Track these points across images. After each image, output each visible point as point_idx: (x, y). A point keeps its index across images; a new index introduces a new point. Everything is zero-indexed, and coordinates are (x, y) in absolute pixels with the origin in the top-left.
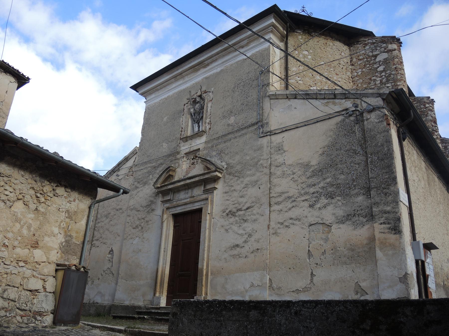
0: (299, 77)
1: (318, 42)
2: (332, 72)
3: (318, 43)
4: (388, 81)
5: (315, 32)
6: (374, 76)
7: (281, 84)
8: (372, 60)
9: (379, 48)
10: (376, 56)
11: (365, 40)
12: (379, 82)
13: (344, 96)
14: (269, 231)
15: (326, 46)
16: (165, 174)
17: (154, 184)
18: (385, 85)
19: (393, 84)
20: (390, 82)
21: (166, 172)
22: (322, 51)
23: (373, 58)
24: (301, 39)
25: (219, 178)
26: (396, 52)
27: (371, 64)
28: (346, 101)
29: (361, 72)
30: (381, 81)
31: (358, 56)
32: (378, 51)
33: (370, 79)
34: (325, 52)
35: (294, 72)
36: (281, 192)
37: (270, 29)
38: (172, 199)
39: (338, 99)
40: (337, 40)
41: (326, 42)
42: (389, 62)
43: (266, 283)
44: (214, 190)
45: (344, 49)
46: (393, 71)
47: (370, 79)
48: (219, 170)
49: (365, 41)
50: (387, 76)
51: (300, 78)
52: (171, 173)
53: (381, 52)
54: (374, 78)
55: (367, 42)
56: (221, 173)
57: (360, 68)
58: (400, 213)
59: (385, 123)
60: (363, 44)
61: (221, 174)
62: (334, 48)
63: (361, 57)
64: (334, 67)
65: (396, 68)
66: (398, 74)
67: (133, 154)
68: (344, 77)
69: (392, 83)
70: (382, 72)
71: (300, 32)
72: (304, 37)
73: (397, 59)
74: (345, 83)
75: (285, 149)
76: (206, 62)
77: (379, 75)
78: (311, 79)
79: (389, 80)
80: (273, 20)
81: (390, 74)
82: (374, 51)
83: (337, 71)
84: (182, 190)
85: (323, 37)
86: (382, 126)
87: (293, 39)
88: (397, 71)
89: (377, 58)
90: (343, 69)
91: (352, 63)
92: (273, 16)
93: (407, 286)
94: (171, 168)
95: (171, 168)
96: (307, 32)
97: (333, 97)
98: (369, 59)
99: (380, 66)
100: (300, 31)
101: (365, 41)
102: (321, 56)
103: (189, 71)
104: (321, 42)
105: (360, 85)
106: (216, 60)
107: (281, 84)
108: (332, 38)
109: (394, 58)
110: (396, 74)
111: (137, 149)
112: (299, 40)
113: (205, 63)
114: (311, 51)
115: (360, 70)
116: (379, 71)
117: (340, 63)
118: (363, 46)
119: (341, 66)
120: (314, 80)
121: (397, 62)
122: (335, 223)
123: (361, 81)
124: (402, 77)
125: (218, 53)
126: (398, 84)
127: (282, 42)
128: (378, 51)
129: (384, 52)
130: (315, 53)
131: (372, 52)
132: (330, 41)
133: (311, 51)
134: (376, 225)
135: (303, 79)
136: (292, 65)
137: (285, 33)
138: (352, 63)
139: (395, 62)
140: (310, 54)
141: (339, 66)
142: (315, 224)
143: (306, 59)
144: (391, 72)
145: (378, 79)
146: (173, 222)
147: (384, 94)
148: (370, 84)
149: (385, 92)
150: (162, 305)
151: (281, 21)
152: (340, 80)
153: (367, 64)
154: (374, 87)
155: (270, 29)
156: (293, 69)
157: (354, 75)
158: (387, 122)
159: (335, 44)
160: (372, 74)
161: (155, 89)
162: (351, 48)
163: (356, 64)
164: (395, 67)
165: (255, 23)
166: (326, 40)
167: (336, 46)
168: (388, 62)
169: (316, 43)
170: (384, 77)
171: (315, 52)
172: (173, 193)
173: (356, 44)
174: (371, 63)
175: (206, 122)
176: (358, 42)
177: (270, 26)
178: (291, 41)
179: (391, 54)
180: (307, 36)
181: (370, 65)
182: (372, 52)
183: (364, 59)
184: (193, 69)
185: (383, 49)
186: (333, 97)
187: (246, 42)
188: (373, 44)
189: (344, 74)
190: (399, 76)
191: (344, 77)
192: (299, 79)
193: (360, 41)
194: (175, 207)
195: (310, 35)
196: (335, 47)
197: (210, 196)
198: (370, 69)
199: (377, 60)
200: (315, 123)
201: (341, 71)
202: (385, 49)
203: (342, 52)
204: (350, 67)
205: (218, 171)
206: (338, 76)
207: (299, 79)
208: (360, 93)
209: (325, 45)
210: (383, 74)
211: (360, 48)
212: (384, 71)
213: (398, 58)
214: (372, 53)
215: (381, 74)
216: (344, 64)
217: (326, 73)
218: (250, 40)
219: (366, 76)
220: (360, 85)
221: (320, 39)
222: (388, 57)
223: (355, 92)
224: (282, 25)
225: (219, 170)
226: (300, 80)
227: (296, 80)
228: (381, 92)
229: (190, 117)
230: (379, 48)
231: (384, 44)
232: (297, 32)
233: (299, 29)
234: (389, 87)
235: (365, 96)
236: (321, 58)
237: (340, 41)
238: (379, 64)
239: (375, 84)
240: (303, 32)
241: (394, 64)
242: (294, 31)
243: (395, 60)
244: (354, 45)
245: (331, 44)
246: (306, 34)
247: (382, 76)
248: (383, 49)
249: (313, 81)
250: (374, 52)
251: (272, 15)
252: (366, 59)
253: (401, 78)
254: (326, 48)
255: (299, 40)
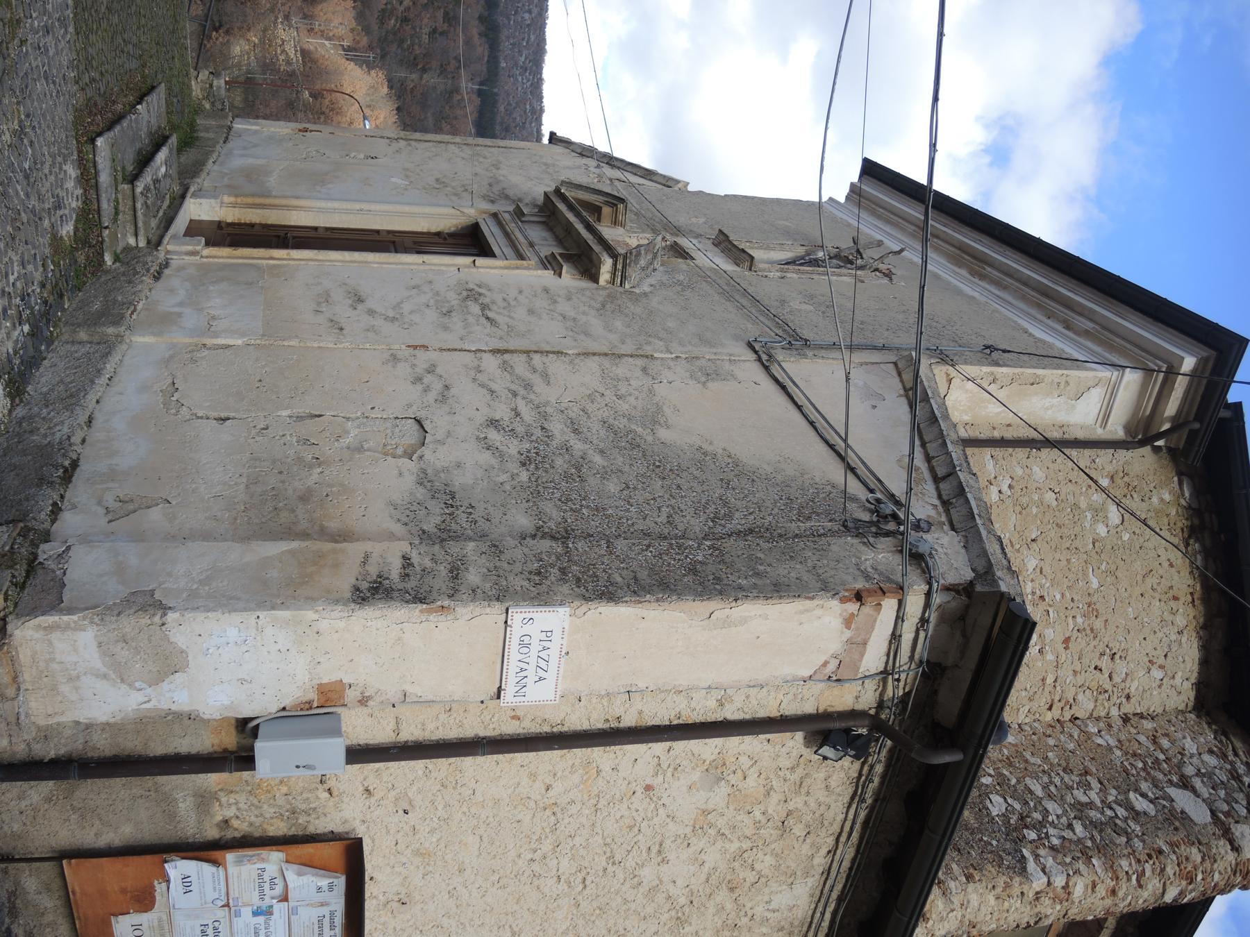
0: (1010, 487)
1: (1171, 565)
2: (1070, 620)
3: (1166, 564)
4: (1092, 825)
5: (1206, 552)
6: (1101, 783)
7: (967, 427)
8: (1165, 775)
9: (1222, 796)
10: (1185, 784)
11: (1241, 753)
12: (1084, 799)
13: (951, 496)
14: (403, 347)
15: (1164, 598)
16: (601, 198)
17: (567, 183)
18: (1075, 818)
19: (1089, 844)
20: (1095, 833)
21: (609, 200)
22: (1139, 578)
23: (1175, 779)
24: (1162, 500)
25: (594, 278)
26: (1226, 852)
27: (1148, 773)
28: (935, 506)
29: (1104, 743)
30: (1087, 804)
31: (1166, 735)
32: (1210, 794)
33: (1087, 772)
34: (1138, 591)
35: (1027, 471)
36: (550, 373)
37: (1157, 365)
38: (523, 219)
39: (937, 489)
40: (1205, 648)
41: (1182, 600)
42: (1176, 829)
43: (292, 553)
44: (553, 269)
45: (1178, 681)
46: (1143, 841)
47: (1087, 772)
48: (619, 267)
49: (1236, 754)
50: (1116, 825)
51: (1009, 494)
52: (606, 210)
53: (1209, 803)
54: (1095, 784)
55: (1231, 757)
56: (613, 282)
57: (1119, 741)
58: (448, 608)
59: (860, 585)
60: (1220, 749)
61: (607, 282)
62: (1165, 630)
63: (1165, 743)
64: (1092, 630)
65: (1160, 852)
66: (1139, 861)
67: (664, 182)
68: (1066, 673)
69: (1092, 838)
70: (1129, 807)
71: (1187, 494)
72: (1174, 512)
73: (1199, 859)
74: (1043, 680)
75: (710, 384)
76: (989, 269)
77: (1111, 798)
78: (1016, 535)
79: (1101, 831)
80: (1189, 363)
81: (1126, 833)
82: (1205, 780)
83: (1082, 642)
84: (554, 233)
85: (1198, 587)
86: (850, 578)
87: (1152, 469)
88: (1150, 856)
89: (1180, 791)
90: (1098, 672)
91: (1134, 720)
92: (1205, 354)
93: (109, 608)
94: (621, 206)
95: (621, 206)
96: (1196, 522)
97: (941, 472)
98: (1165, 766)
99: (1151, 801)
100: (1190, 495)
101: (1236, 754)
102: (1119, 574)
103: (948, 246)
104: (1176, 577)
105: (1051, 742)
106: (1004, 288)
107: (967, 427)
108: (1205, 627)
109: (1200, 843)
110: (1134, 851)
111: (680, 185)
112: (1155, 491)
113: (984, 269)
114: (1126, 537)
115: (1113, 742)
116: (1127, 799)
117: (1117, 657)
118: (1215, 749)
119: (1105, 663)
120: (1017, 546)
121: (1187, 859)
122: (424, 466)
123: (1071, 746)
124: (1129, 880)
125: (1026, 282)
126: (1094, 861)
127: (1126, 433)
128: (1210, 794)
129: (1213, 813)
130: (1121, 549)
131: (1199, 773)
132: (1191, 617)
133: (1126, 537)
134: (404, 547)
135: (1008, 502)
136: (1051, 466)
137: (1166, 426)
138: (1134, 720)
139: (1183, 847)
140: (1113, 531)
141: (1102, 654)
142: (421, 430)
143: (1089, 515)
144: (1137, 836)
145: (1094, 796)
146: (453, 229)
147: (994, 582)
148: (1064, 770)
149: (1001, 583)
150: (194, 203)
151: (1199, 399)
152: (1050, 657)
153: (1145, 763)
154: (1058, 784)
155: (1157, 365)
156: (1036, 469)
157: (1086, 726)
158: (868, 591)
159: (1184, 639)
160: (1108, 776)
161: (874, 206)
162: (1193, 716)
163: (1133, 731)
164: (1164, 848)
165: (1160, 325)
166: (1189, 598)
167: (1180, 644)
168: (1177, 824)
169: (1163, 558)
170: (1109, 813)
171: (1128, 552)
172: (543, 223)
173: (1214, 727)
174: (1152, 772)
175: (785, 272)
176: (1225, 734)
177: (1164, 361)
178: (1142, 461)
179: (1214, 834)
180: (1180, 525)
181: (1144, 769)
182: (1199, 773)
183: (1162, 751)
184: (958, 252)
185: (1225, 807)
186: (941, 472)
187: (1089, 325)
188: (1232, 775)
189: (1080, 679)
190: (1130, 864)
191: (1066, 673)
192: (1005, 488)
193: (1228, 738)
194: (507, 235)
195: (1190, 537)
196: (1173, 637)
197: (533, 262)
198: (1126, 771)
199: (1173, 792)
200: (827, 442)
201: (1086, 661)
202: (1227, 814)
203: (1161, 667)
204: (1114, 712)
205: (615, 265)
206: (1060, 647)
207: (1005, 488)
208: (976, 525)
209: (1170, 595)
210: (1121, 812)
211: (1202, 740)
212: (1136, 815)
213: (1203, 859)
214: (1197, 775)
215: (1121, 806)
216: (1117, 679)
217: (1058, 597)
218: (1098, 332)
219: (1093, 759)
220: (1051, 742)
221: (1185, 572)
222: (1195, 824)
223: (976, 511)
224: (1185, 410)
225: (619, 267)
226: (1000, 492)
227: (995, 478)
228: (999, 574)
229: (799, 255)
230: (1222, 796)
231: (1245, 811)
232: (1180, 483)
233: (1196, 492)
234: (1073, 830)
235: (967, 542)
236: (1113, 573)
237: (1204, 663)
238: (1157, 798)
239: (1070, 788)
240: (1189, 508)
241: (1173, 845)
242: (1180, 474)
243: (1194, 850)
244: (1209, 724)
245: (1181, 621)
246: (1187, 519)
247: (1111, 808)
248: (1225, 807)
249: (1013, 540)
250: (1202, 781)
251: (1206, 352)
252: (1162, 757)
253: (1122, 875)
254: (1157, 596)
255: (1155, 491)
